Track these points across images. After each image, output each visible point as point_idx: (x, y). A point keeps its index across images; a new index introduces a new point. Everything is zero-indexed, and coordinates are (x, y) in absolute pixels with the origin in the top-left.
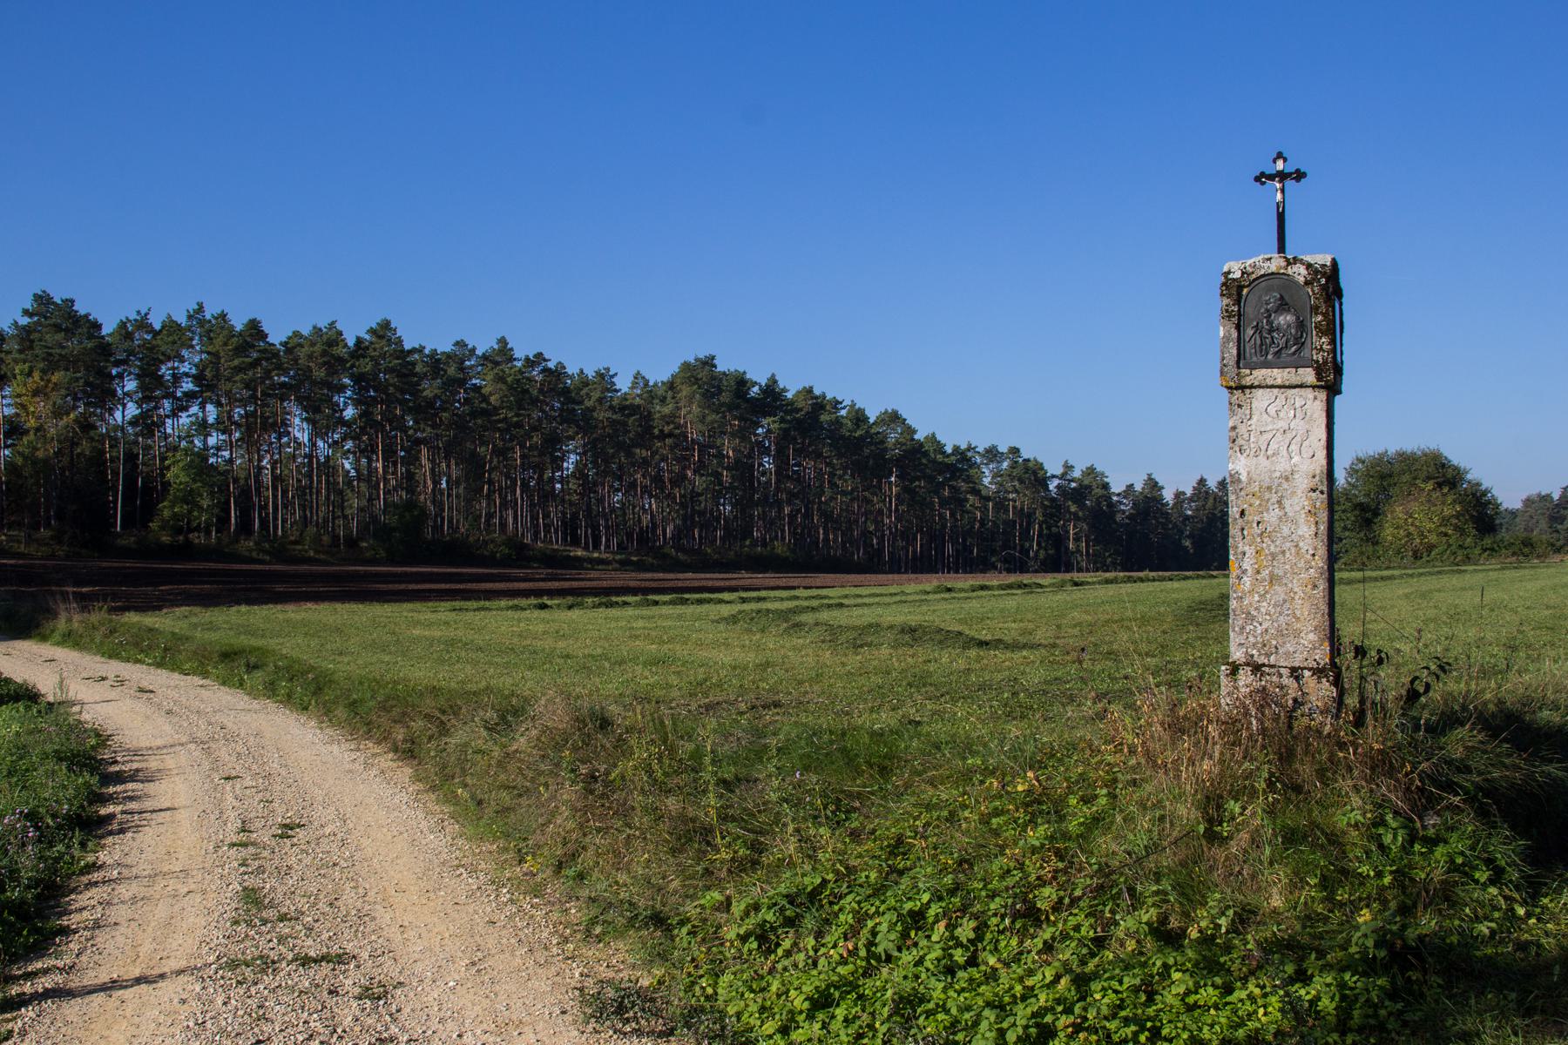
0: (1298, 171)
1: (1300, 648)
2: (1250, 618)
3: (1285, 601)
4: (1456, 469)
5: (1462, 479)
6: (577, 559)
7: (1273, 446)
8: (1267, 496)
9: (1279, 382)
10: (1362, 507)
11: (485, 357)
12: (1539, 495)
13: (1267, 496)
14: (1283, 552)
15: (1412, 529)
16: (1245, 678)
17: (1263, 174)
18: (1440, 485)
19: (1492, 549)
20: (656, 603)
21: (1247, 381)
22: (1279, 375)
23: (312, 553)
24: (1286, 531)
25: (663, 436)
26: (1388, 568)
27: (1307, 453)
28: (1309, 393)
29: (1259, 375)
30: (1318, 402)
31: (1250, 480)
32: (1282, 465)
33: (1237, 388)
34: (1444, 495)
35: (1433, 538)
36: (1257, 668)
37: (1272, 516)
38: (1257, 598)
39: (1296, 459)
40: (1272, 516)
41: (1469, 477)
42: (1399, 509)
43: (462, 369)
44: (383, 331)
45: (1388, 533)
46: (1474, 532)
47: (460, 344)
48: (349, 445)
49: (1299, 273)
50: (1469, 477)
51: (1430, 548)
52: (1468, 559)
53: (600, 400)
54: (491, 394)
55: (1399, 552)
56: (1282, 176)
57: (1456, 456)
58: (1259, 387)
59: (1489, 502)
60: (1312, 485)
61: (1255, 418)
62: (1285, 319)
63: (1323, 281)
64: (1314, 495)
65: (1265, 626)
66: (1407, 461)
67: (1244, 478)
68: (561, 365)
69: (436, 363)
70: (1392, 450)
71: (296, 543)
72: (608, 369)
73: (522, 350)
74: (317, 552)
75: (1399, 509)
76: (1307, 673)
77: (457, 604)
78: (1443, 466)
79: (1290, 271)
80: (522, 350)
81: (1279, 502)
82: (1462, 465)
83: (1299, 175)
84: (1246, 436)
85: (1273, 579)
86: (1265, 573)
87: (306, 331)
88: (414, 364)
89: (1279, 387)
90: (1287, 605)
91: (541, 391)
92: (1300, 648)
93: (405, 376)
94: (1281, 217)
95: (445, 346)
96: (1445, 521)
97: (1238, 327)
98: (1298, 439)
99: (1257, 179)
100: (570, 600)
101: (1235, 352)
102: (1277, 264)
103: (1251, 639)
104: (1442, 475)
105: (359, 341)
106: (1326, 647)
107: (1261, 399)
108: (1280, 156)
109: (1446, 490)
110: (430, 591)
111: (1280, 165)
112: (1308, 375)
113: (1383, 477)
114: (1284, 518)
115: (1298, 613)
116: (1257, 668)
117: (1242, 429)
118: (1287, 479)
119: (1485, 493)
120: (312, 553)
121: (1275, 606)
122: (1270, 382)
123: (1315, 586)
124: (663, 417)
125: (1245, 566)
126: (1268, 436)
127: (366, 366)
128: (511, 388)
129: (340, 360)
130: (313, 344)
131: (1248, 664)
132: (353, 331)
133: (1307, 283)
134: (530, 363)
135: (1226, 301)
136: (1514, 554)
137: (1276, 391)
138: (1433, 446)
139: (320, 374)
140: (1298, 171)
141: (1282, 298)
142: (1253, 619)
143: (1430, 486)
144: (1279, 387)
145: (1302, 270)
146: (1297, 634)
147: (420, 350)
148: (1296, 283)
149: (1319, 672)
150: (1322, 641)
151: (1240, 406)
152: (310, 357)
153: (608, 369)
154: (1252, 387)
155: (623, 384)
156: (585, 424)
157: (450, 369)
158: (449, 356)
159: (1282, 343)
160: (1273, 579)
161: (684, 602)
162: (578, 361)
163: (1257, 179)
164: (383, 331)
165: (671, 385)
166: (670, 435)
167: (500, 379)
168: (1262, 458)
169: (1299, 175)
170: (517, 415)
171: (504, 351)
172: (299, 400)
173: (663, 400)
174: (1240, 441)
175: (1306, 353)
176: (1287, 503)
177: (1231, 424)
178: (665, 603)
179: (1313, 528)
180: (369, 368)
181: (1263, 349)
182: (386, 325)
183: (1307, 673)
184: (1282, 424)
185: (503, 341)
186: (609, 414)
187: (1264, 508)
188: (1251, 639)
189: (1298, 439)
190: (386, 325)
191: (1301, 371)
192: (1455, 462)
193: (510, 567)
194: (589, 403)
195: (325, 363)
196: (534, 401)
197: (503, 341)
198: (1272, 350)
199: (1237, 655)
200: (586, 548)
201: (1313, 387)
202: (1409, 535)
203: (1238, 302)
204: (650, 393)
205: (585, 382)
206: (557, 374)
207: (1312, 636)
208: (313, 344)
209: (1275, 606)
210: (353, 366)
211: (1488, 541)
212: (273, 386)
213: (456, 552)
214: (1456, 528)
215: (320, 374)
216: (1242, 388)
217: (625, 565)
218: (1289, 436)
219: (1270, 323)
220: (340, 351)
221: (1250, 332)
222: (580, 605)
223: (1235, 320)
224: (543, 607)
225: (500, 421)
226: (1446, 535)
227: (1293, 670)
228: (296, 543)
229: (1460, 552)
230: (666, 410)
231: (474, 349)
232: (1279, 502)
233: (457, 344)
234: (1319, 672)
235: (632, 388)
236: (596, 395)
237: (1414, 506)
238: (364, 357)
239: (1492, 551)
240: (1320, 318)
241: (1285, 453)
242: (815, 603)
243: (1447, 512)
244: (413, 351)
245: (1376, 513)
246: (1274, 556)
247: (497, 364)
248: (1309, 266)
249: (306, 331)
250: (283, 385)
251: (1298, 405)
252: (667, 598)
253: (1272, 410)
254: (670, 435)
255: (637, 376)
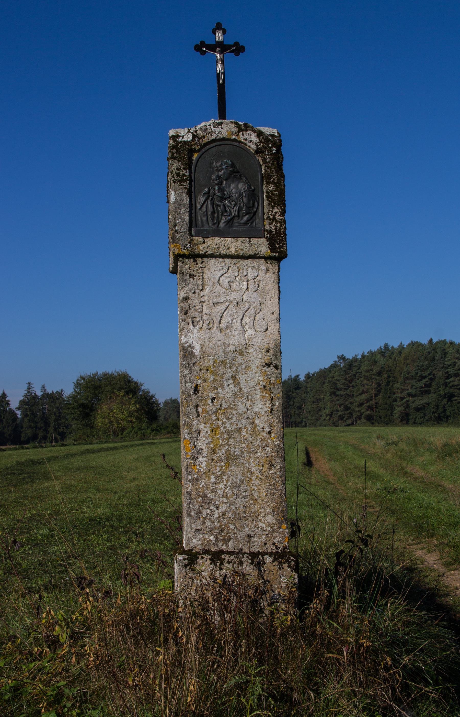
0: (236, 44)
1: (259, 531)
3: (242, 482)
4: (136, 383)
5: (140, 389)
7: (227, 318)
8: (221, 370)
9: (233, 251)
10: (83, 406)
12: (171, 399)
13: (221, 370)
14: (239, 430)
15: (112, 419)
16: (205, 565)
17: (203, 44)
18: (127, 393)
19: (157, 430)
21: (201, 249)
22: (232, 245)
24: (241, 408)
26: (106, 442)
27: (260, 327)
28: (262, 265)
29: (213, 243)
30: (270, 275)
31: (204, 353)
32: (236, 339)
33: (189, 257)
34: (130, 399)
35: (124, 424)
36: (216, 557)
38: (213, 480)
39: (250, 332)
40: (227, 391)
41: (143, 388)
42: (105, 407)
45: (99, 421)
46: (147, 420)
49: (251, 139)
50: (143, 388)
51: (123, 429)
52: (143, 437)
55: (105, 433)
56: (223, 47)
57: (136, 377)
58: (213, 256)
59: (154, 403)
60: (266, 360)
61: (207, 289)
62: (236, 188)
64: (268, 369)
65: (222, 509)
66: (108, 379)
67: (197, 351)
70: (100, 372)
75: (105, 407)
76: (268, 559)
78: (129, 381)
79: (241, 137)
81: (234, 377)
82: (139, 381)
83: (238, 49)
84: (198, 308)
85: (230, 459)
86: (221, 452)
89: (232, 257)
90: (245, 486)
92: (259, 531)
94: (221, 89)
96: (131, 414)
97: (189, 193)
98: (251, 311)
99: (198, 48)
101: (187, 218)
102: (226, 130)
103: (208, 524)
104: (126, 386)
106: (285, 530)
107: (214, 269)
108: (219, 27)
109: (131, 396)
111: (219, 36)
112: (262, 246)
113: (95, 388)
114: (239, 394)
115: (255, 494)
116: (216, 557)
117: (195, 300)
118: (241, 353)
119: (152, 397)
121: (232, 487)
122: (223, 251)
123: (272, 466)
125: (200, 445)
131: (206, 552)
133: (258, 151)
135: (176, 165)
136: (168, 433)
137: (228, 261)
138: (123, 370)
140: (236, 44)
141: (233, 165)
142: (210, 501)
143: (122, 394)
144: (232, 257)
145: (254, 137)
146: (255, 517)
148: (248, 151)
149: (280, 556)
151: (192, 276)
154: (205, 256)
159: (234, 211)
160: (230, 459)
163: (198, 48)
168: (215, 331)
169: (238, 49)
174: (193, 313)
175: (258, 223)
176: (242, 378)
177: (182, 294)
179: (268, 404)
181: (215, 216)
183: (268, 559)
184: (234, 296)
187: (219, 383)
188: (208, 524)
189: (251, 311)
191: (254, 241)
192: (135, 379)
198: (224, 220)
201: (266, 258)
202: (111, 422)
203: (189, 166)
207: (270, 519)
209: (232, 487)
211: (154, 426)
214: (137, 418)
216: (194, 256)
218: (243, 308)
219: (222, 190)
221: (201, 199)
223: (186, 184)
226: (131, 422)
227: (253, 555)
229: (139, 432)
232: (234, 377)
234: (280, 556)
237: (114, 405)
239: (157, 431)
240: (272, 187)
241: (238, 325)
243: (132, 408)
245: (92, 410)
246: (229, 434)
248: (260, 134)
251: (250, 276)
253: (225, 281)
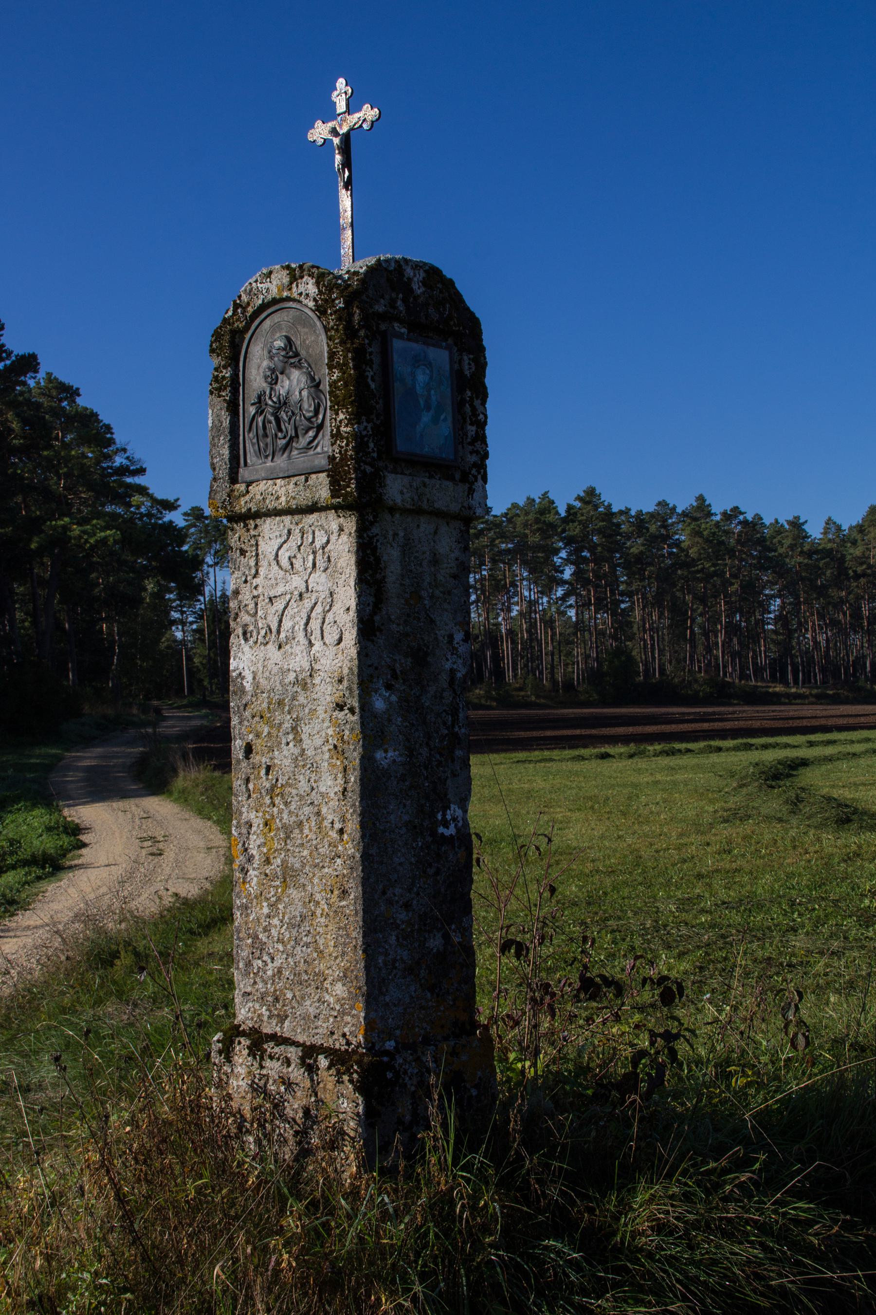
2: (259, 947)
6: (776, 695)
7: (287, 624)
11: (685, 514)
14: (300, 824)
20: (719, 749)
23: (533, 698)
24: (303, 786)
25: (857, 577)
27: (331, 637)
28: (332, 520)
32: (298, 661)
37: (284, 757)
39: (318, 646)
40: (284, 757)
43: (665, 526)
44: (590, 497)
47: (662, 504)
48: (572, 601)
53: (792, 547)
54: (689, 547)
61: (262, 571)
63: (340, 304)
64: (341, 715)
68: (758, 517)
69: (641, 522)
71: (520, 689)
72: (798, 518)
73: (719, 507)
74: (538, 697)
76: (323, 1062)
77: (522, 755)
80: (719, 507)
81: (294, 729)
87: (521, 503)
88: (618, 525)
90: (306, 927)
91: (738, 541)
93: (610, 536)
95: (649, 507)
98: (319, 609)
100: (632, 747)
105: (570, 508)
110: (591, 737)
118: (305, 687)
120: (533, 698)
124: (856, 559)
126: (279, 605)
127: (574, 530)
128: (707, 541)
129: (552, 526)
130: (527, 514)
132: (564, 499)
134: (728, 517)
135: (216, 361)
139: (534, 539)
146: (320, 981)
147: (626, 512)
150: (353, 997)
152: (526, 525)
153: (798, 518)
155: (815, 531)
156: (778, 567)
157: (655, 526)
158: (652, 515)
161: (748, 747)
162: (771, 509)
164: (590, 497)
165: (860, 529)
166: (864, 575)
167: (697, 533)
168: (272, 648)
170: (714, 565)
171: (702, 508)
172: (525, 563)
173: (854, 543)
178: (728, 749)
179: (340, 781)
180: (577, 530)
182: (591, 492)
185: (701, 499)
186: (800, 559)
190: (591, 492)
193: (712, 704)
194: (781, 550)
195: (539, 529)
196: (731, 552)
197: (701, 499)
199: (244, 1013)
200: (787, 684)
204: (846, 540)
205: (778, 529)
206: (753, 526)
207: (340, 989)
208: (527, 514)
210: (564, 531)
212: (501, 552)
213: (663, 692)
215: (534, 539)
217: (821, 699)
218: (307, 603)
220: (550, 518)
222: (641, 753)
223: (226, 394)
224: (605, 756)
225: (698, 572)
228: (520, 689)
230: (858, 552)
231: (674, 508)
233: (659, 504)
235: (825, 533)
236: (787, 542)
238: (573, 521)
242: (829, 750)
244: (621, 512)
247: (695, 519)
249: (521, 503)
250: (509, 551)
252: (730, 743)
254: (864, 575)
255: (829, 521)
